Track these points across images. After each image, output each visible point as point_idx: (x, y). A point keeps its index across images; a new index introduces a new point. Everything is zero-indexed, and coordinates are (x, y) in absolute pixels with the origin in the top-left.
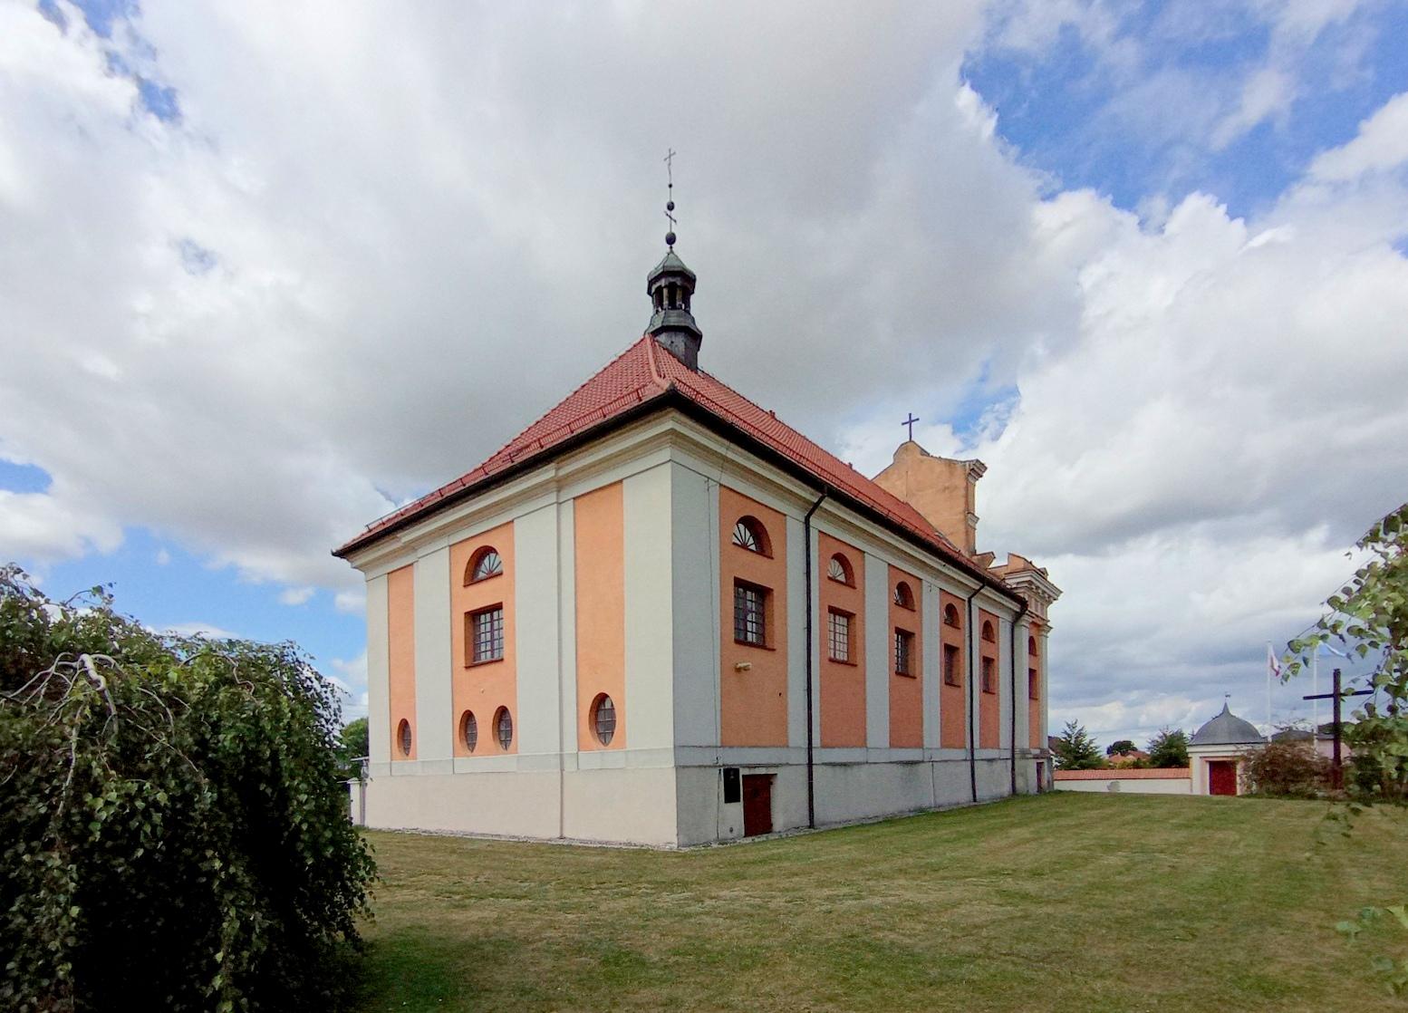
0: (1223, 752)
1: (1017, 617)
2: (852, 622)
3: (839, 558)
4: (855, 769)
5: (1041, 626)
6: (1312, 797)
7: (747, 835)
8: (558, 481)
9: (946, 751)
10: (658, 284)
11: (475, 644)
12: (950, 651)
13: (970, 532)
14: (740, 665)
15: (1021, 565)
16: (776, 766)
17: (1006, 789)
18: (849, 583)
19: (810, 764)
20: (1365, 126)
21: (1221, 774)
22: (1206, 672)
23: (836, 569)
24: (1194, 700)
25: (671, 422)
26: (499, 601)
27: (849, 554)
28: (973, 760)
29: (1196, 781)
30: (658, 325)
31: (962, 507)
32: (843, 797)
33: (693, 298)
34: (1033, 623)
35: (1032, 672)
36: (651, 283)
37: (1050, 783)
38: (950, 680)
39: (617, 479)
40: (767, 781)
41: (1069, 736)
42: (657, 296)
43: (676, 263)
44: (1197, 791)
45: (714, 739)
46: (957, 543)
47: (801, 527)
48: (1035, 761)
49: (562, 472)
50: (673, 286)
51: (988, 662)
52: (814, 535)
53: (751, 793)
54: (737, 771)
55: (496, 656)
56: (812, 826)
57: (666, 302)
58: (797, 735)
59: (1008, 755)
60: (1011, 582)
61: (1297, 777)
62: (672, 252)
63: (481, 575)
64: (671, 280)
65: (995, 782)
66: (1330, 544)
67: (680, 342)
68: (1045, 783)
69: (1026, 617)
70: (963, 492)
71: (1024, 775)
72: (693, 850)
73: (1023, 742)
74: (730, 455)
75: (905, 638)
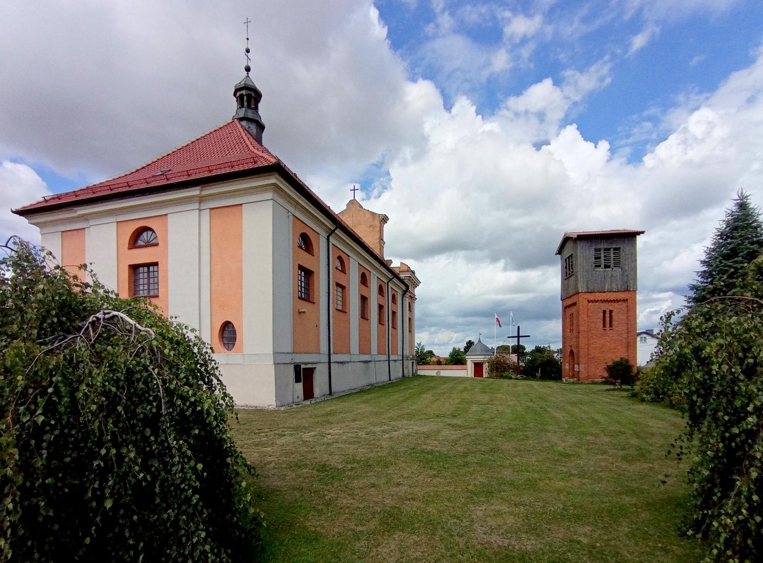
0: (479, 359)
1: (405, 292)
2: (344, 291)
3: (340, 258)
4: (346, 365)
5: (413, 298)
6: (511, 378)
7: (304, 400)
8: (200, 197)
9: (380, 356)
10: (241, 92)
11: (135, 285)
12: (381, 307)
13: (381, 248)
14: (301, 310)
15: (406, 268)
16: (316, 363)
17: (400, 375)
18: (343, 271)
19: (330, 363)
20: (589, 142)
21: (478, 367)
22: (461, 320)
23: (338, 264)
24: (456, 332)
25: (273, 179)
26: (156, 261)
27: (344, 257)
28: (389, 360)
29: (467, 372)
30: (242, 115)
31: (378, 236)
32: (348, 377)
33: (260, 105)
34: (410, 296)
35: (410, 319)
36: (237, 91)
37: (416, 373)
38: (381, 322)
39: (239, 203)
40: (312, 371)
41: (418, 349)
42: (240, 100)
43: (251, 84)
44: (469, 376)
45: (290, 350)
46: (376, 251)
47: (325, 241)
48: (411, 361)
49: (205, 193)
50: (248, 96)
51: (394, 313)
52: (331, 244)
53: (304, 375)
54: (300, 365)
55: (152, 293)
56: (330, 394)
57: (245, 104)
58: (324, 349)
59: (400, 358)
60: (402, 276)
61: (505, 370)
62: (248, 76)
63: (140, 243)
64: (249, 92)
65: (397, 373)
66: (505, 269)
67: (253, 129)
68: (414, 371)
69: (408, 293)
70: (378, 229)
71: (407, 368)
72: (286, 407)
73: (407, 353)
74: (300, 201)
75: (364, 299)
